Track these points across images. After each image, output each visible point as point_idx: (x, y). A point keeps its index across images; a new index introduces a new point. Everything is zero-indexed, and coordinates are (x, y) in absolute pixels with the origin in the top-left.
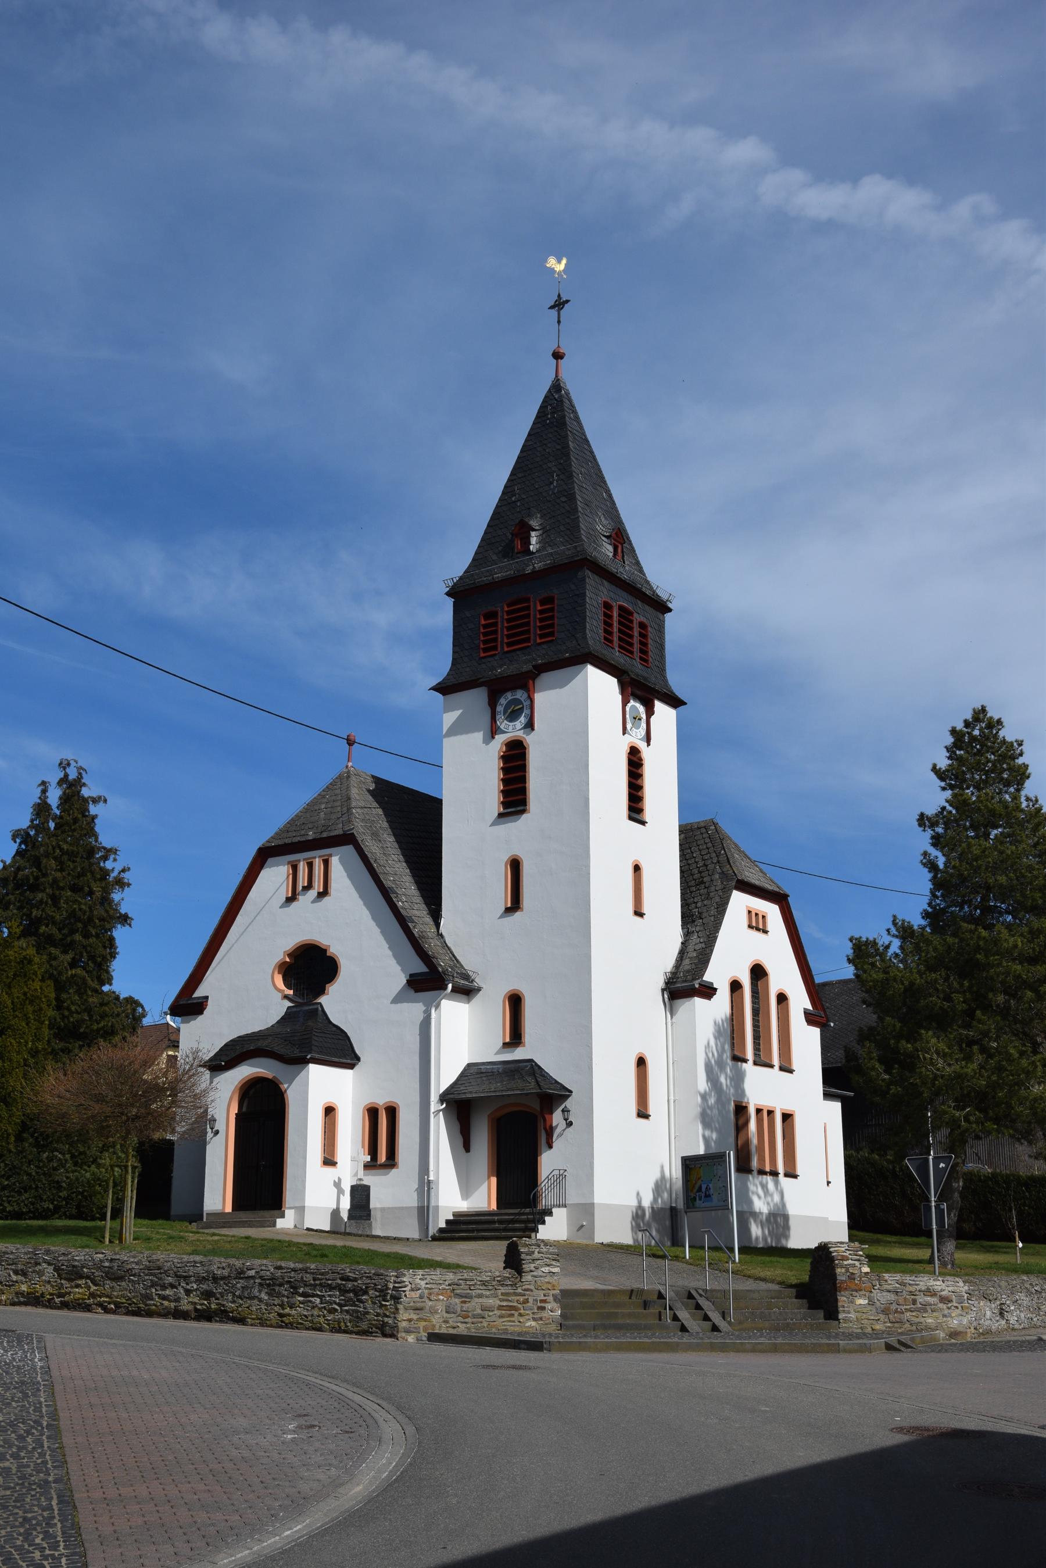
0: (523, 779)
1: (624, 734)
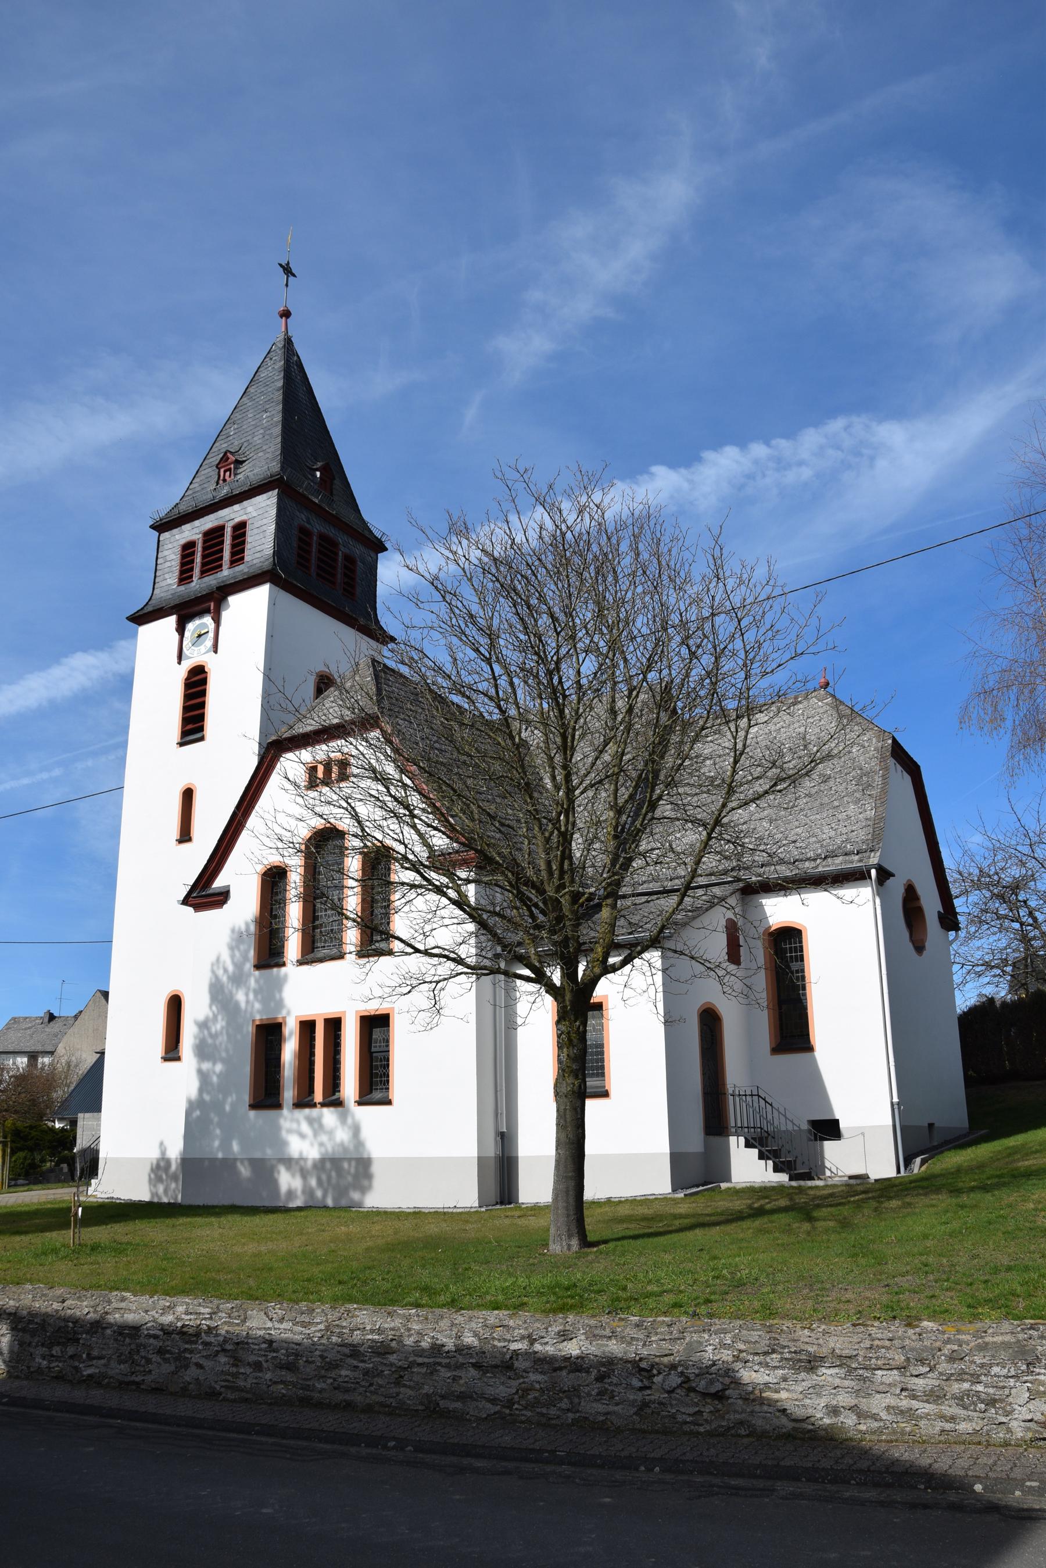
0: (186, 709)
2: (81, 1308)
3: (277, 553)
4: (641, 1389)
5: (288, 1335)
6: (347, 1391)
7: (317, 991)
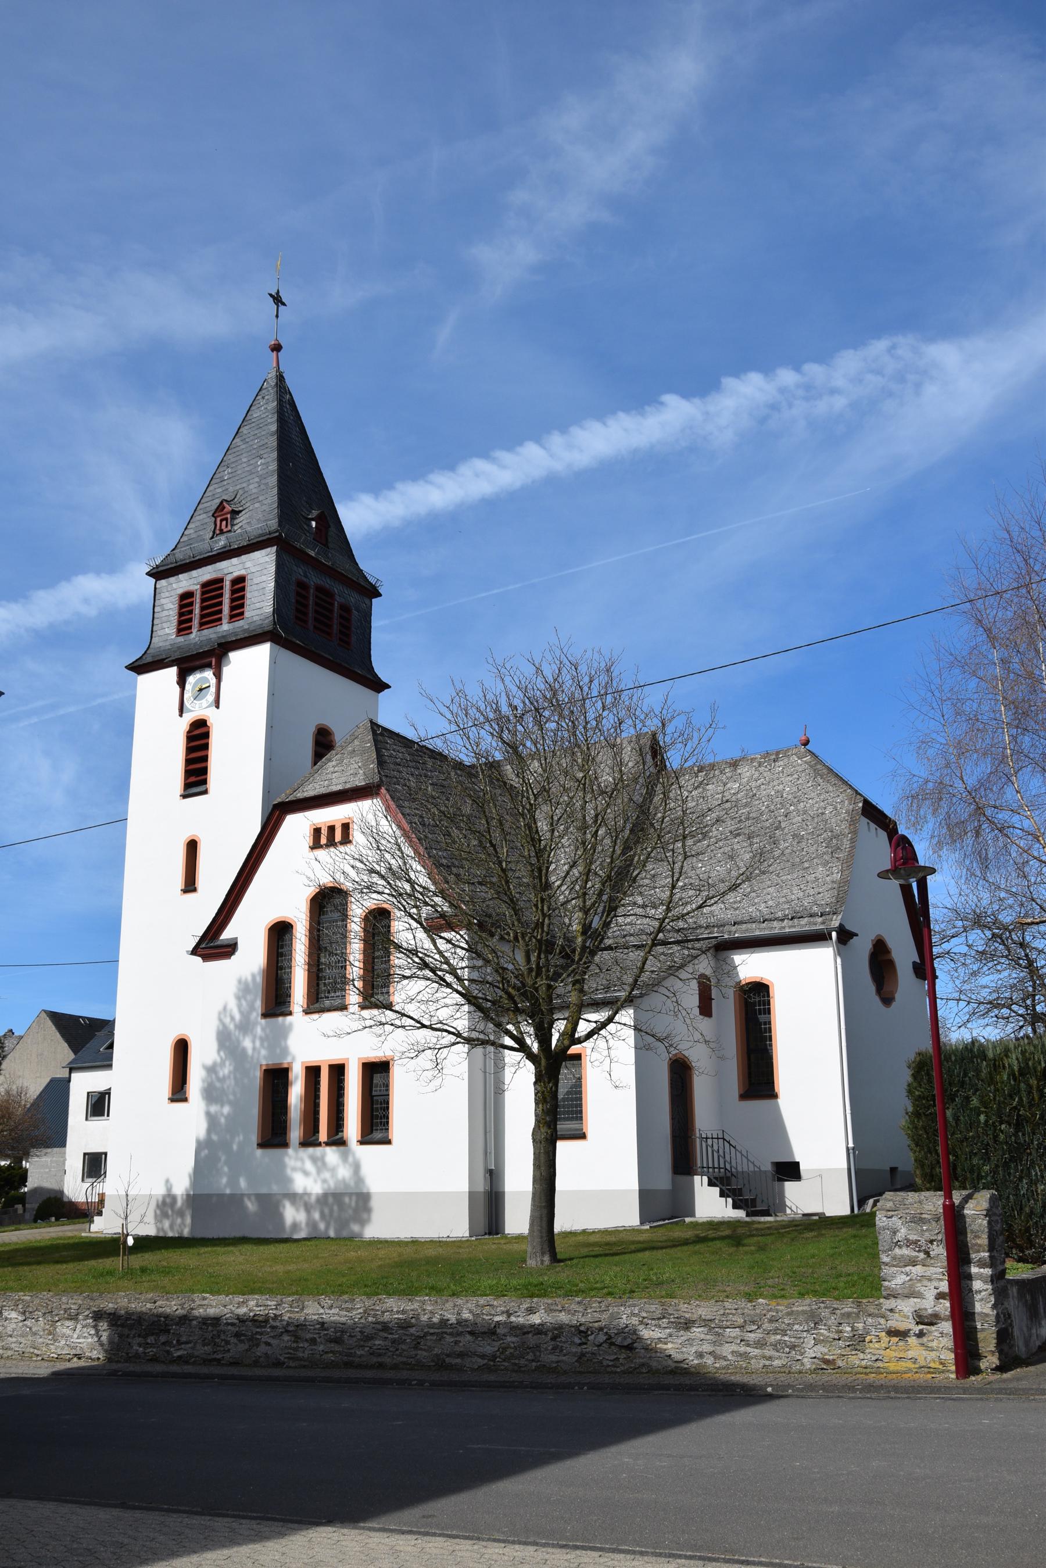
0: (188, 762)
2: (171, 1307)
3: (277, 610)
4: (580, 1344)
5: (336, 1318)
6: (380, 1355)
7: (315, 1039)
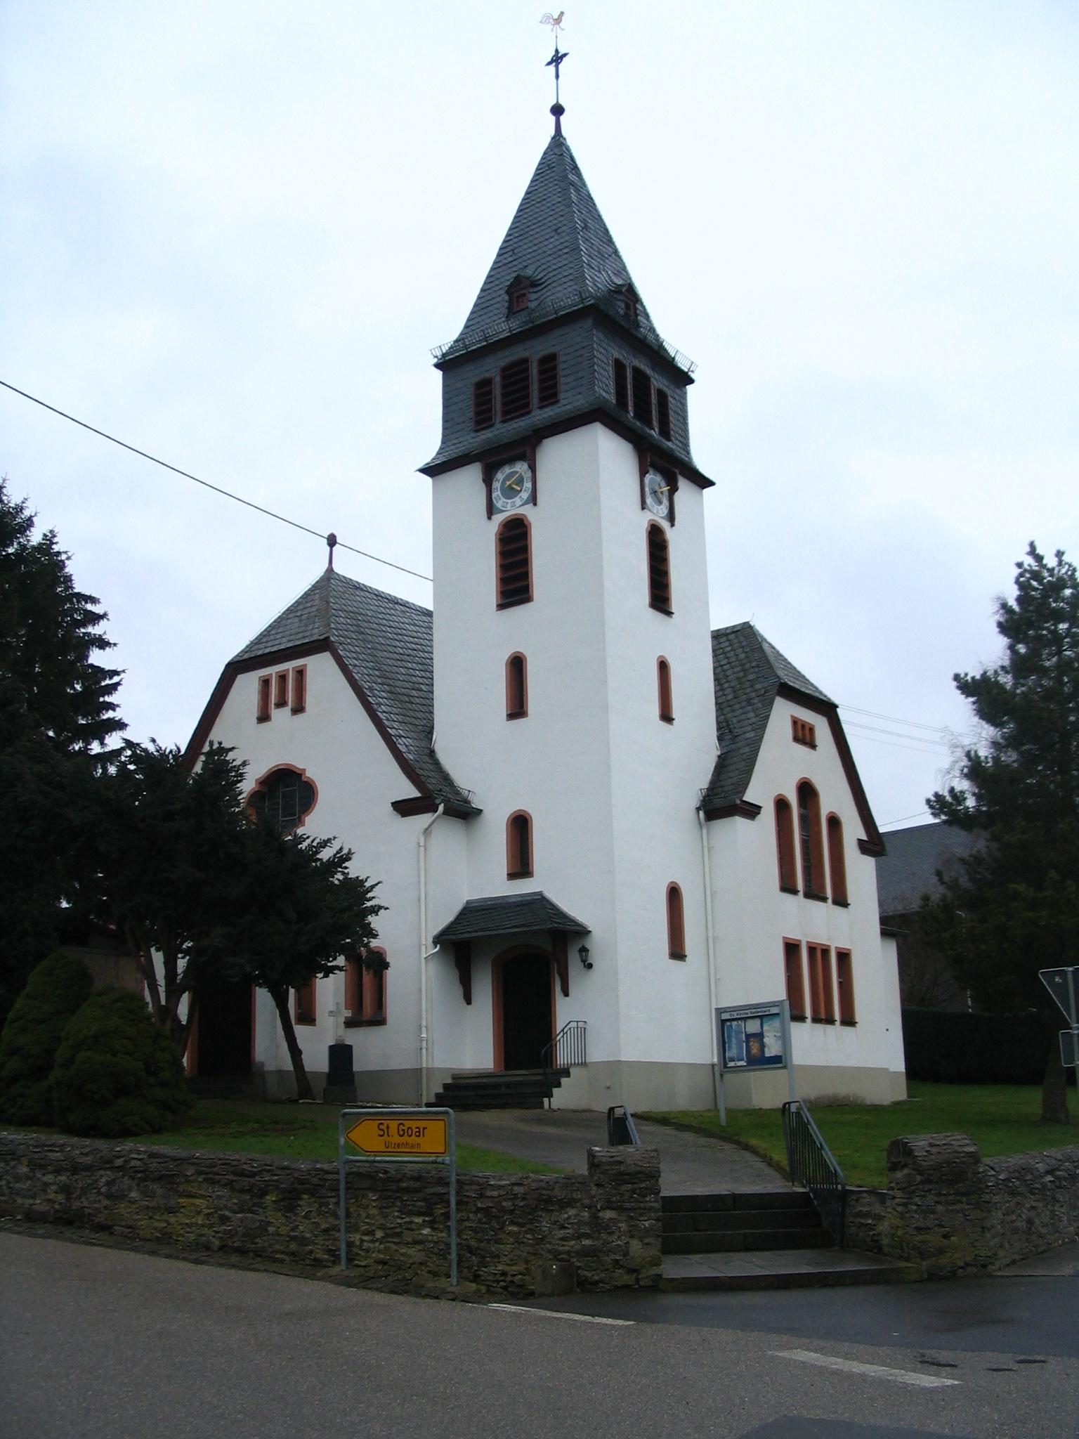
1: (643, 508)
